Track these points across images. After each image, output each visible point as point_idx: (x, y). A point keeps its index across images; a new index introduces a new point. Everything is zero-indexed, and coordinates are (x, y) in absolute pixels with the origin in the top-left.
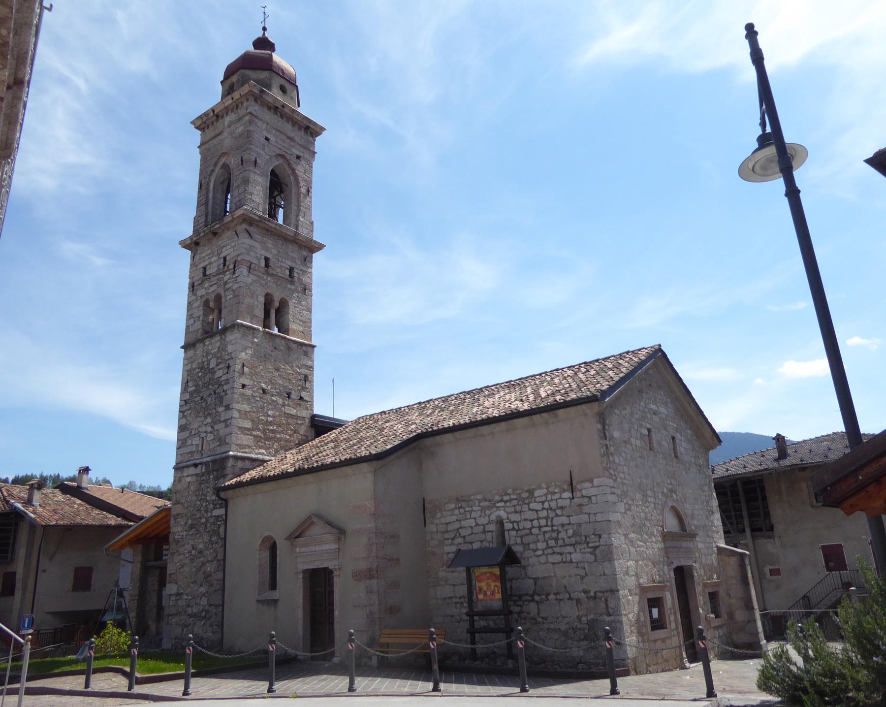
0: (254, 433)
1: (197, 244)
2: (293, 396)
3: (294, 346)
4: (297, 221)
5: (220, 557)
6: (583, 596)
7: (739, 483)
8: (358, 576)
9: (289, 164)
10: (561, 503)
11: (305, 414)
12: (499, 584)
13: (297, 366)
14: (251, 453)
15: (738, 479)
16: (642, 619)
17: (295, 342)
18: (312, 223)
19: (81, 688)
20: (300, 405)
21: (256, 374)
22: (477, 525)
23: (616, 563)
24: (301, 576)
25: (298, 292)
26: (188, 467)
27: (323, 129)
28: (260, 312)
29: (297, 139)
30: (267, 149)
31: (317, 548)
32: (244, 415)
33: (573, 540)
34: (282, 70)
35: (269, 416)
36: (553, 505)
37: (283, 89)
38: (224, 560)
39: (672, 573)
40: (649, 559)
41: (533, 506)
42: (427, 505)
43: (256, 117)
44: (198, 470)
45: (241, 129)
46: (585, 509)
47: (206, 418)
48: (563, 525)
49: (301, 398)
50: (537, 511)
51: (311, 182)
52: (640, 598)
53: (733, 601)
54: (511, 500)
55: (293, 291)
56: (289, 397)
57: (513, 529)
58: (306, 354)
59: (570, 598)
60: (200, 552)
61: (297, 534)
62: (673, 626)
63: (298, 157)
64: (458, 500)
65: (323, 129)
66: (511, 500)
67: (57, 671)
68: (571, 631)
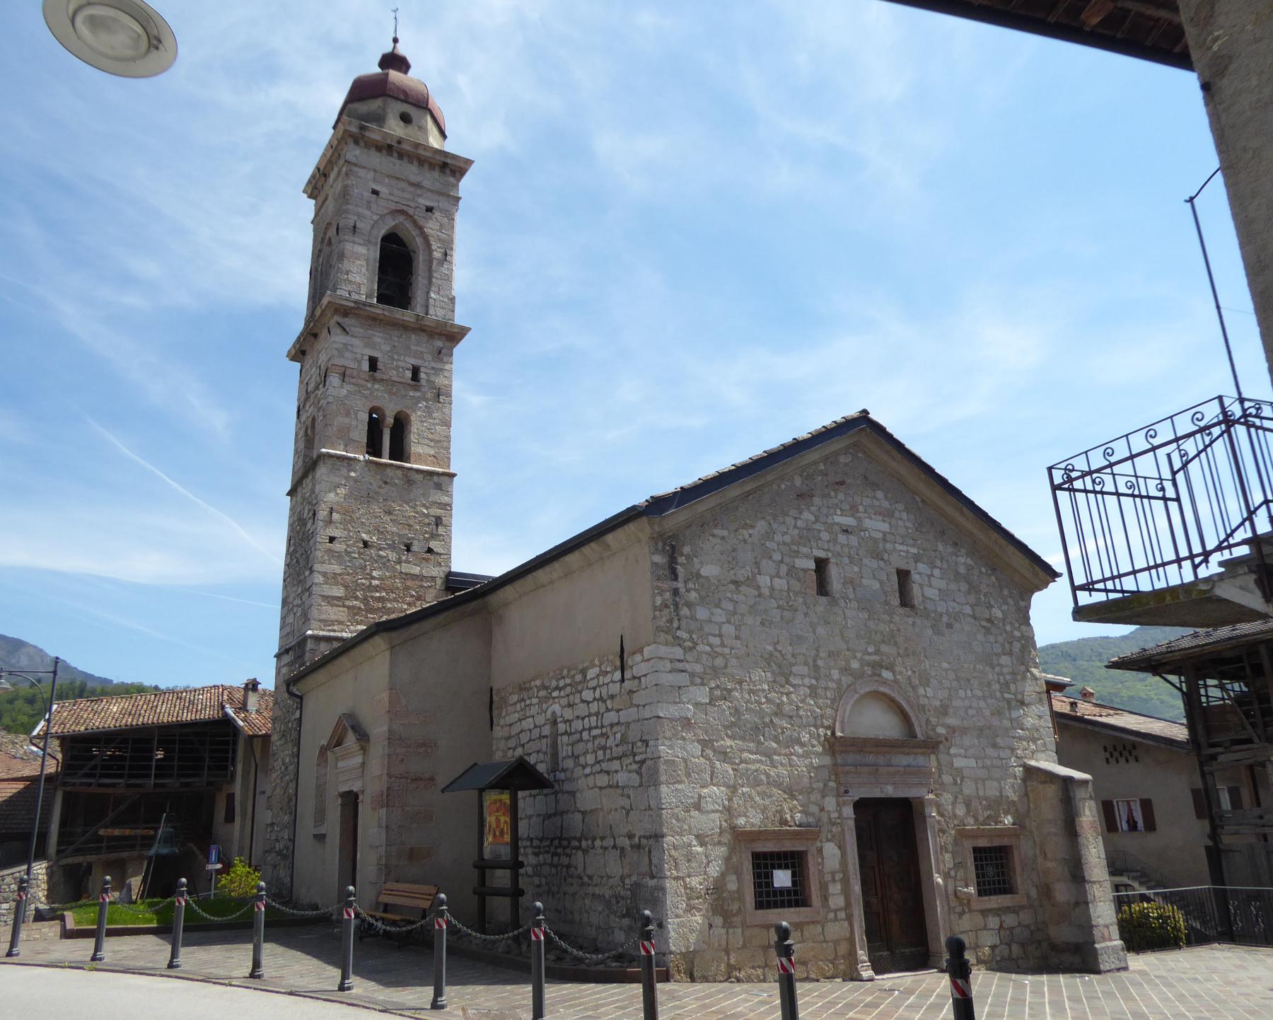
0: (347, 603)
1: (303, 353)
2: (414, 548)
3: (420, 477)
4: (428, 298)
7: (1263, 650)
9: (415, 222)
11: (438, 572)
12: (508, 820)
13: (424, 506)
14: (342, 631)
15: (1262, 642)
16: (732, 885)
17: (418, 471)
18: (453, 300)
20: (427, 560)
21: (352, 520)
23: (664, 789)
25: (427, 400)
27: (469, 162)
28: (361, 435)
29: (426, 183)
30: (374, 207)
32: (332, 578)
33: (620, 750)
34: (405, 92)
35: (373, 578)
37: (406, 119)
39: (849, 811)
40: (778, 785)
42: (495, 698)
43: (355, 165)
46: (637, 699)
49: (430, 551)
50: (588, 703)
51: (451, 242)
52: (732, 851)
53: (1050, 864)
55: (418, 400)
56: (408, 550)
58: (439, 487)
59: (614, 847)
62: (837, 901)
63: (429, 209)
65: (469, 162)
68: (614, 901)
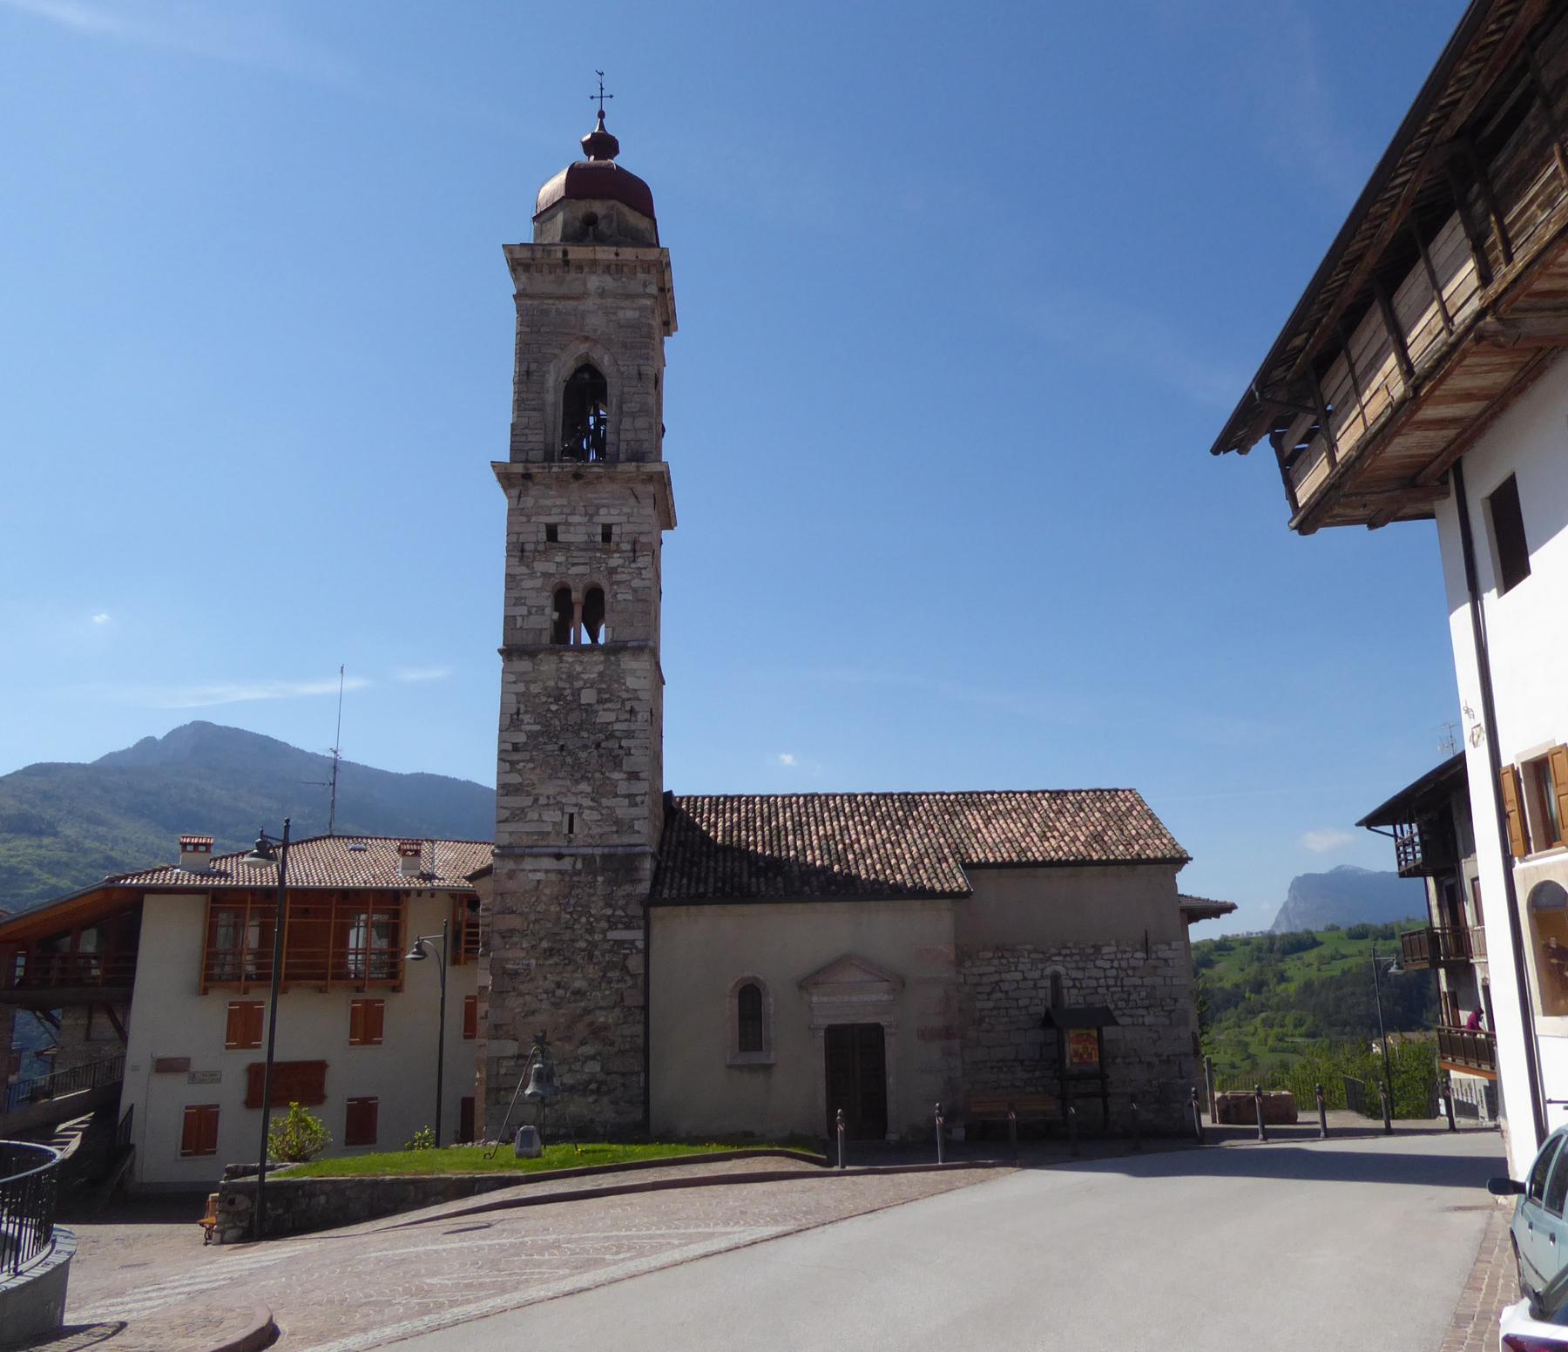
5: (634, 999)
10: (1133, 963)
22: (1025, 979)
24: (822, 1034)
31: (854, 999)
33: (1146, 1003)
36: (1124, 964)
38: (645, 1008)
41: (1099, 963)
44: (566, 864)
45: (630, 314)
47: (577, 782)
48: (1135, 987)
54: (1071, 955)
57: (1074, 986)
59: (1140, 1062)
61: (808, 982)
65: (508, 248)
66: (1071, 955)
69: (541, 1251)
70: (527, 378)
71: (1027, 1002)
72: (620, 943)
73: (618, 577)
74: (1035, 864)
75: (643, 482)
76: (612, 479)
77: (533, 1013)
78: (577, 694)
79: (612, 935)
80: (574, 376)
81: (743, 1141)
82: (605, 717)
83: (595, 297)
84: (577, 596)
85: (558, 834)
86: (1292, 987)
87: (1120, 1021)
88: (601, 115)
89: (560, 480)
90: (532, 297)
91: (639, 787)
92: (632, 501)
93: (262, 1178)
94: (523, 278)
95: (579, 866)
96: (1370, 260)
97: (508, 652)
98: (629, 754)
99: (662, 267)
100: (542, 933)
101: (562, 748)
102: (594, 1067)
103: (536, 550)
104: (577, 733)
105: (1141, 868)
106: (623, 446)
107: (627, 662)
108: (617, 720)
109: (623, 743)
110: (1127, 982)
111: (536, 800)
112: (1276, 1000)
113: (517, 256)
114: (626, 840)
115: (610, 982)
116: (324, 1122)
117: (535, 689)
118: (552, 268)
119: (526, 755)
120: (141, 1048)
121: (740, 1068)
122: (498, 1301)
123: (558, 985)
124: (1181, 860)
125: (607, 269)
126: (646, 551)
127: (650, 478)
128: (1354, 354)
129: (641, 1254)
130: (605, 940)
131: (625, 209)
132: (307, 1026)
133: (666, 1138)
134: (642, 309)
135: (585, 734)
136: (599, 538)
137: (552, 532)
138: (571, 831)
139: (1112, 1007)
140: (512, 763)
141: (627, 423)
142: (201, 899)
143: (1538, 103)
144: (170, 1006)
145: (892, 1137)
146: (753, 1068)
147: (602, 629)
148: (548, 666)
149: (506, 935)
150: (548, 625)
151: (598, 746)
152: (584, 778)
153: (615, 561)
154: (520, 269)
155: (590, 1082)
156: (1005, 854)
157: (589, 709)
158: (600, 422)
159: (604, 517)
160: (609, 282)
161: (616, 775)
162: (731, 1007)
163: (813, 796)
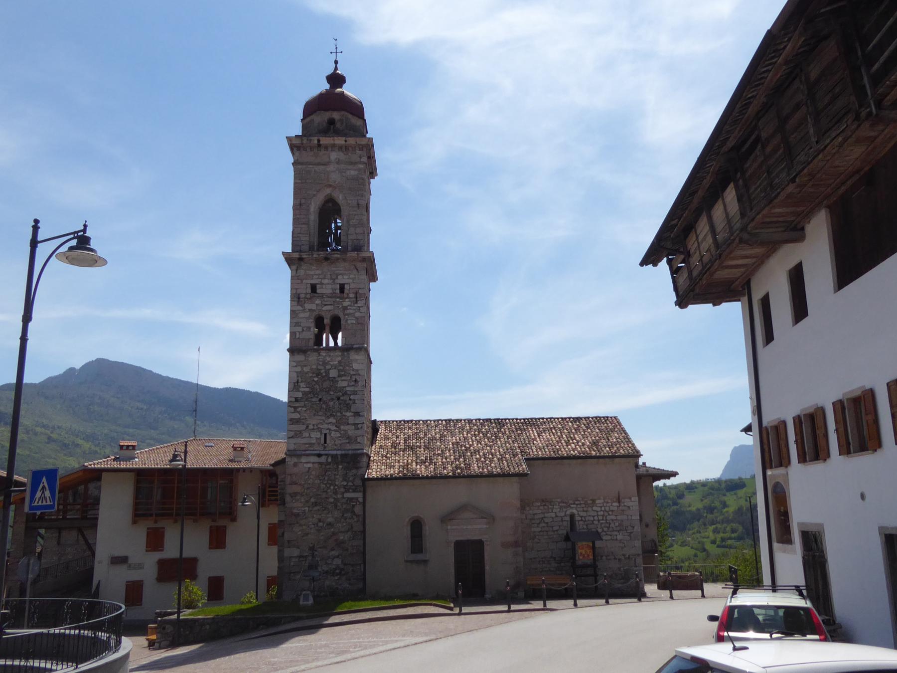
6: (622, 558)
8: (505, 545)
10: (612, 508)
19: (542, 607)
26: (308, 455)
31: (469, 527)
33: (618, 529)
36: (607, 509)
45: (353, 173)
47: (328, 417)
59: (615, 559)
60: (330, 524)
61: (447, 518)
64: (543, 501)
65: (289, 139)
67: (339, 611)
69: (320, 647)
70: (299, 207)
71: (557, 528)
72: (351, 499)
73: (348, 312)
74: (563, 458)
75: (360, 261)
76: (344, 260)
77: (307, 534)
78: (327, 372)
79: (347, 495)
80: (324, 205)
81: (413, 597)
82: (342, 384)
83: (335, 166)
84: (327, 321)
85: (319, 444)
86: (731, 510)
87: (604, 538)
88: (336, 62)
89: (317, 260)
90: (302, 164)
91: (358, 420)
92: (355, 272)
93: (178, 616)
94: (297, 153)
95: (330, 460)
96: (700, 193)
97: (292, 350)
98: (354, 403)
99: (369, 147)
100: (311, 494)
101: (320, 400)
102: (338, 562)
103: (306, 298)
104: (328, 392)
105: (617, 460)
106: (350, 243)
107: (353, 356)
108: (349, 386)
109: (352, 397)
110: (609, 518)
111: (307, 427)
112: (721, 517)
113: (294, 142)
114: (354, 447)
115: (346, 519)
116: (197, 590)
117: (306, 369)
118: (312, 148)
119: (302, 404)
120: (103, 552)
121: (411, 562)
122: (308, 666)
123: (320, 520)
124: (640, 455)
125: (340, 148)
126: (362, 297)
127: (364, 260)
128: (698, 232)
129: (366, 648)
130: (343, 498)
131: (350, 116)
132: (188, 540)
133: (374, 597)
134: (359, 170)
135: (332, 393)
136: (338, 291)
137: (314, 288)
138: (325, 442)
139: (600, 530)
140: (295, 408)
141: (352, 230)
142: (132, 474)
143: (759, 147)
144: (115, 527)
145: (487, 596)
146: (418, 562)
147: (340, 335)
148: (313, 357)
149: (294, 495)
150: (312, 337)
151: (338, 399)
152: (332, 415)
153: (346, 303)
154: (295, 149)
155: (336, 569)
156: (547, 452)
157: (334, 380)
158: (337, 228)
159: (341, 280)
160: (342, 156)
161: (348, 414)
162: (407, 531)
163: (450, 420)
